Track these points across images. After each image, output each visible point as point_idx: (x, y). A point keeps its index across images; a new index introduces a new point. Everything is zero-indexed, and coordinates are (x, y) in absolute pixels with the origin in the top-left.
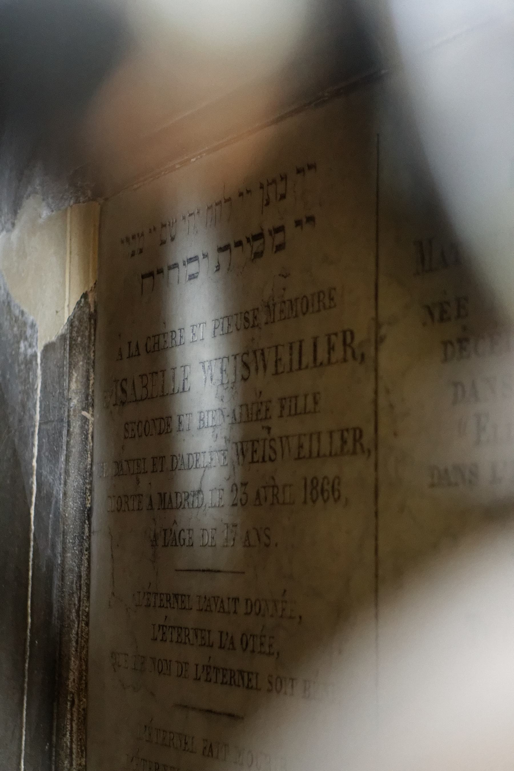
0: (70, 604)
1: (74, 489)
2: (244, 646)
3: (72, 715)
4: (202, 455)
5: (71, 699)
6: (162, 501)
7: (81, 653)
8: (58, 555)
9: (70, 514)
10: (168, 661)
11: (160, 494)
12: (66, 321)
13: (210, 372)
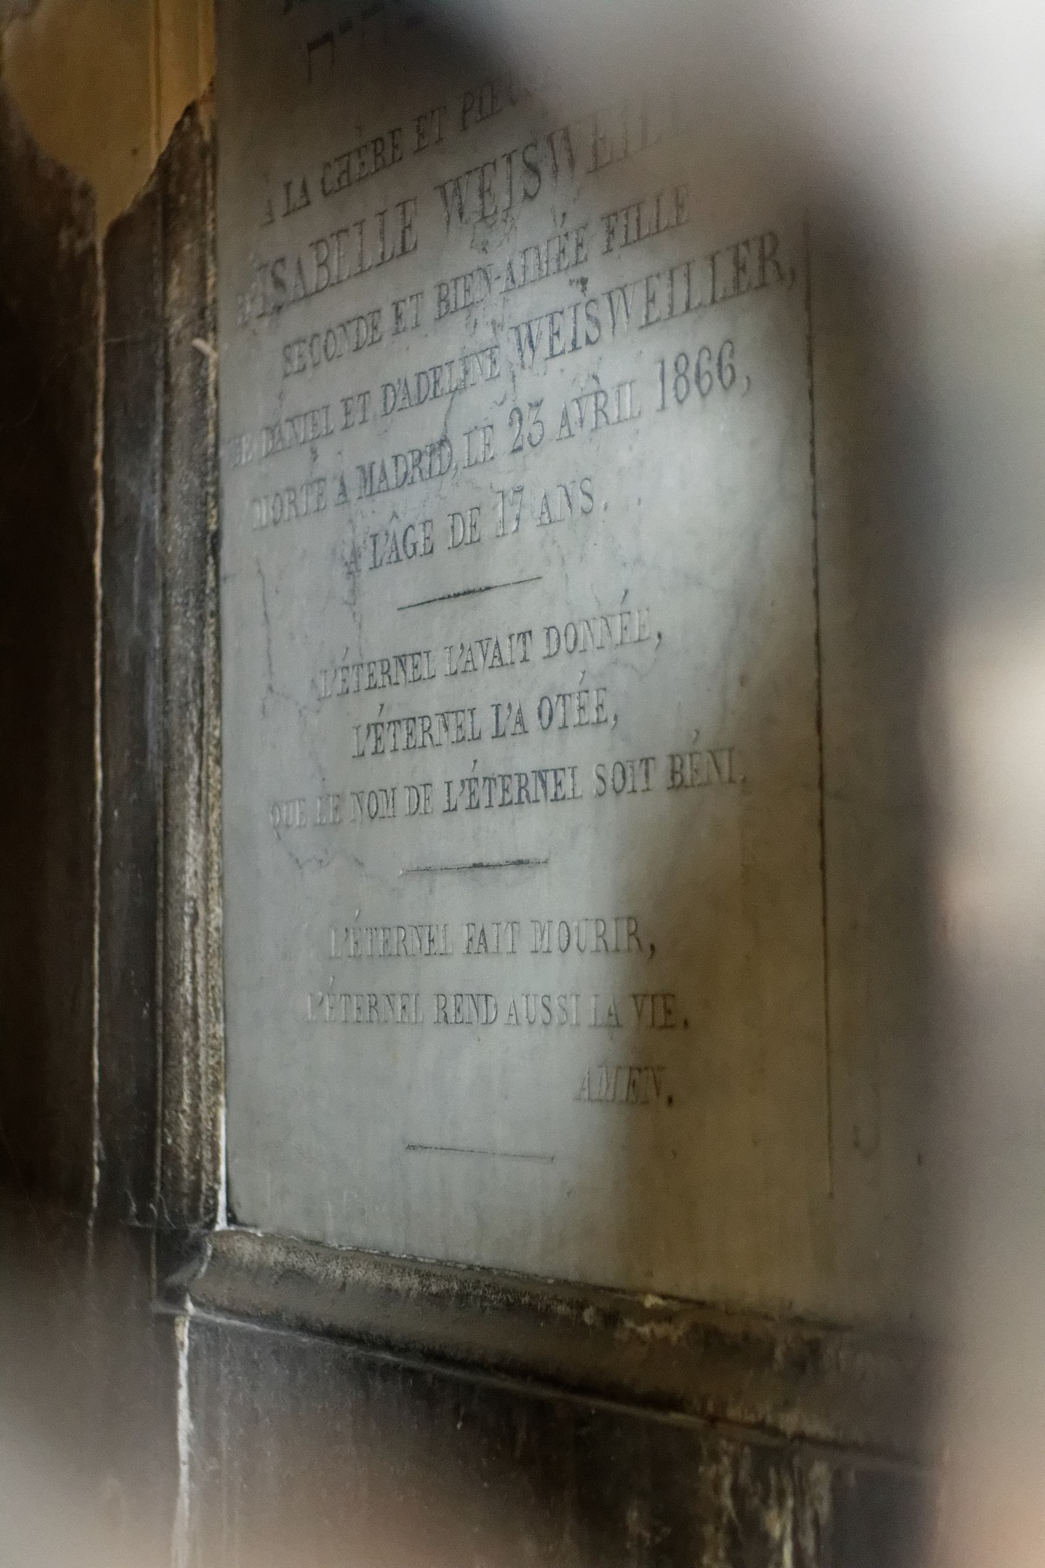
0: (182, 726)
1: (183, 498)
2: (546, 721)
3: (194, 941)
4: (446, 369)
5: (192, 911)
6: (366, 481)
7: (207, 817)
8: (155, 632)
9: (175, 547)
10: (389, 790)
11: (361, 468)
12: (153, 166)
13: (457, 200)
